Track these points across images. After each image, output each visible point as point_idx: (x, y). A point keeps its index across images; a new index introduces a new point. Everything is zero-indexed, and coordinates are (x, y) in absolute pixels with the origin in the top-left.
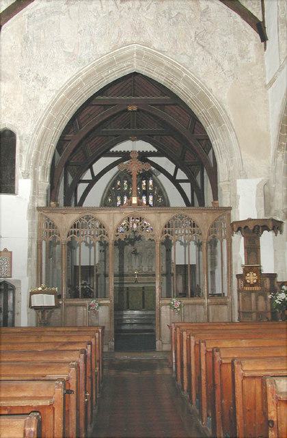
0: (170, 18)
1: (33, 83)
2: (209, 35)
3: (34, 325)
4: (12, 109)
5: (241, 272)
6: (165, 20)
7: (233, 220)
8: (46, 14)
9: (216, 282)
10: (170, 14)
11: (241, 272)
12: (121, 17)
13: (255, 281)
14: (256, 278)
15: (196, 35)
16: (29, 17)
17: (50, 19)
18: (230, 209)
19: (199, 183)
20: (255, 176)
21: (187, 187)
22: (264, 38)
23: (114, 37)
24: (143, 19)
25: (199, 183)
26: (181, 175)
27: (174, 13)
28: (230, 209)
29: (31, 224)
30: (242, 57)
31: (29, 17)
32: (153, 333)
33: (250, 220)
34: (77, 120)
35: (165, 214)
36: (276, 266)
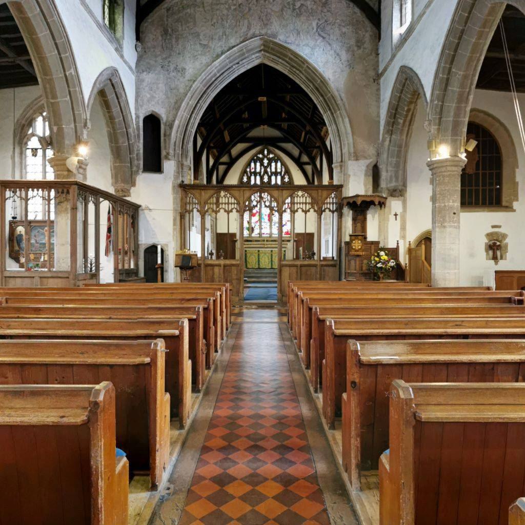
0: (294, 9)
1: (173, 74)
2: (330, 27)
3: (179, 281)
4: (155, 97)
5: (347, 239)
6: (289, 12)
7: (344, 195)
8: (183, 7)
9: (519, 270)
10: (294, 5)
11: (347, 239)
12: (250, 9)
13: (360, 247)
14: (361, 244)
15: (318, 27)
16: (168, 10)
17: (186, 11)
18: (341, 186)
19: (319, 166)
20: (366, 158)
21: (309, 168)
22: (396, 220)
23: (244, 29)
24: (269, 11)
25: (319, 166)
26: (305, 159)
27: (298, 5)
28: (341, 186)
29: (175, 199)
30: (359, 47)
31: (168, 10)
32: (322, 279)
33: (357, 196)
34: (218, 116)
35: (287, 191)
36: (379, 235)
